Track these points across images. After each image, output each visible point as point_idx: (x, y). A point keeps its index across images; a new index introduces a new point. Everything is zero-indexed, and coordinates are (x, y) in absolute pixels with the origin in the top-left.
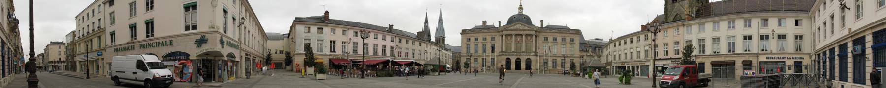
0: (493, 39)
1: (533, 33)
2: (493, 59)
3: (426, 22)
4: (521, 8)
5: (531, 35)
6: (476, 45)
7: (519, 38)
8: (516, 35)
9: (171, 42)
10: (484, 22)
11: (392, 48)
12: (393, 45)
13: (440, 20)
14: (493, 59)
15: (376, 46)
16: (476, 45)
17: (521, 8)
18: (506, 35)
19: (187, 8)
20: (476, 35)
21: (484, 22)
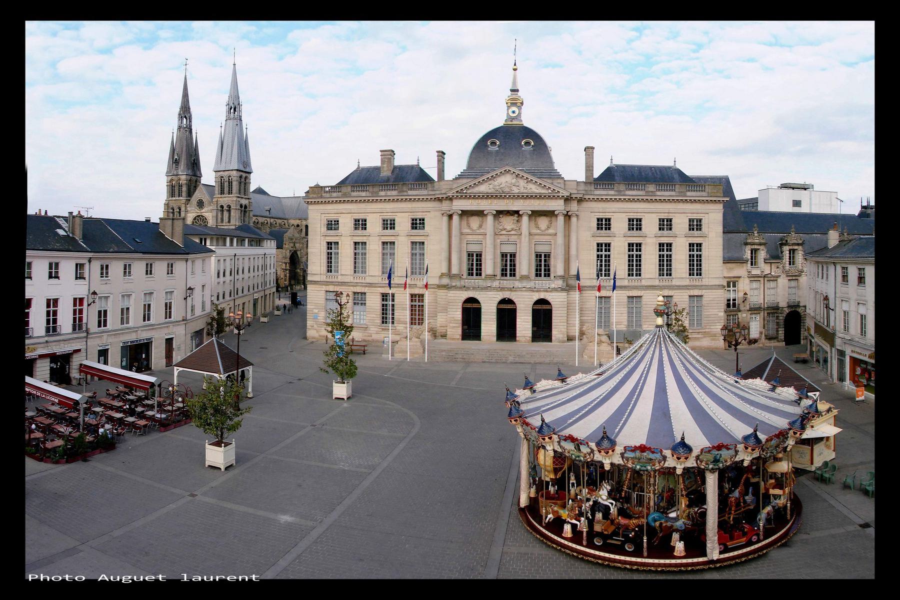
0: (418, 224)
1: (557, 205)
2: (417, 298)
3: (185, 112)
4: (515, 102)
5: (551, 214)
6: (418, 246)
7: (508, 223)
8: (499, 213)
9: (190, 289)
10: (388, 155)
11: (78, 302)
12: (81, 289)
13: (234, 108)
14: (417, 298)
15: (52, 303)
16: (418, 246)
17: (515, 102)
18: (465, 214)
19: (512, 91)
20: (331, 211)
21: (388, 155)
